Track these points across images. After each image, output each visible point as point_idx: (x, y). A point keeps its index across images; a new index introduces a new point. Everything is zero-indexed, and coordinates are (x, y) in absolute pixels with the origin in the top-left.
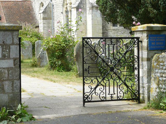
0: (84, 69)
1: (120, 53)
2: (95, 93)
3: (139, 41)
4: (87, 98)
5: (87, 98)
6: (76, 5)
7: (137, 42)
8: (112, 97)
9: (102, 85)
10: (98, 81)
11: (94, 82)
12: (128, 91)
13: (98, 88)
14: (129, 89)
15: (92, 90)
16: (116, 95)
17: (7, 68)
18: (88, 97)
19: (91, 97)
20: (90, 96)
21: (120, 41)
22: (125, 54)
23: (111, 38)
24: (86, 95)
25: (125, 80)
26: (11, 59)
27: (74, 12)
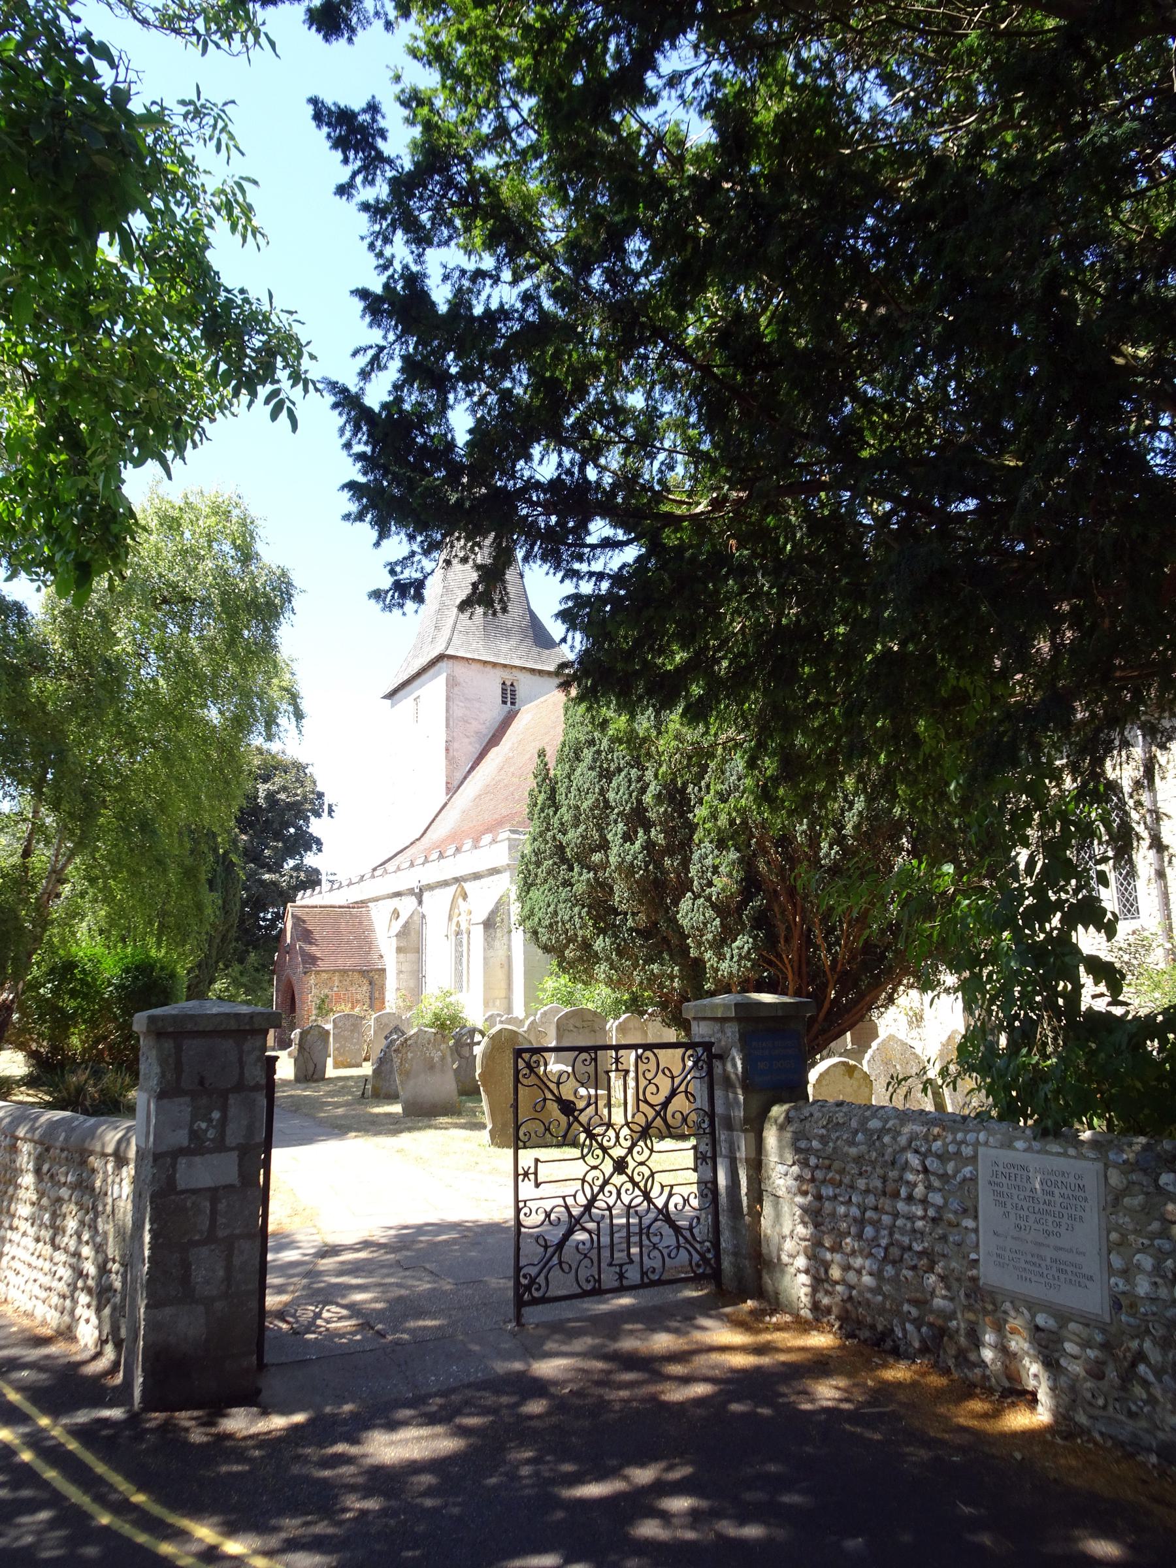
0: (521, 1171)
1: (646, 1101)
2: (673, 1078)
3: (711, 1057)
4: (528, 1288)
5: (528, 1288)
6: (484, 916)
7: (704, 1057)
8: (621, 1276)
9: (652, 1106)
10: (665, 1120)
11: (678, 1115)
12: (678, 1247)
13: (665, 1091)
14: (681, 1240)
15: (550, 1250)
16: (636, 1266)
17: (209, 1189)
18: (533, 1281)
19: (543, 1284)
20: (541, 1280)
21: (588, 1281)
22: (666, 1104)
23: (617, 1048)
24: (525, 1276)
25: (570, 1125)
26: (232, 1149)
27: (478, 932)
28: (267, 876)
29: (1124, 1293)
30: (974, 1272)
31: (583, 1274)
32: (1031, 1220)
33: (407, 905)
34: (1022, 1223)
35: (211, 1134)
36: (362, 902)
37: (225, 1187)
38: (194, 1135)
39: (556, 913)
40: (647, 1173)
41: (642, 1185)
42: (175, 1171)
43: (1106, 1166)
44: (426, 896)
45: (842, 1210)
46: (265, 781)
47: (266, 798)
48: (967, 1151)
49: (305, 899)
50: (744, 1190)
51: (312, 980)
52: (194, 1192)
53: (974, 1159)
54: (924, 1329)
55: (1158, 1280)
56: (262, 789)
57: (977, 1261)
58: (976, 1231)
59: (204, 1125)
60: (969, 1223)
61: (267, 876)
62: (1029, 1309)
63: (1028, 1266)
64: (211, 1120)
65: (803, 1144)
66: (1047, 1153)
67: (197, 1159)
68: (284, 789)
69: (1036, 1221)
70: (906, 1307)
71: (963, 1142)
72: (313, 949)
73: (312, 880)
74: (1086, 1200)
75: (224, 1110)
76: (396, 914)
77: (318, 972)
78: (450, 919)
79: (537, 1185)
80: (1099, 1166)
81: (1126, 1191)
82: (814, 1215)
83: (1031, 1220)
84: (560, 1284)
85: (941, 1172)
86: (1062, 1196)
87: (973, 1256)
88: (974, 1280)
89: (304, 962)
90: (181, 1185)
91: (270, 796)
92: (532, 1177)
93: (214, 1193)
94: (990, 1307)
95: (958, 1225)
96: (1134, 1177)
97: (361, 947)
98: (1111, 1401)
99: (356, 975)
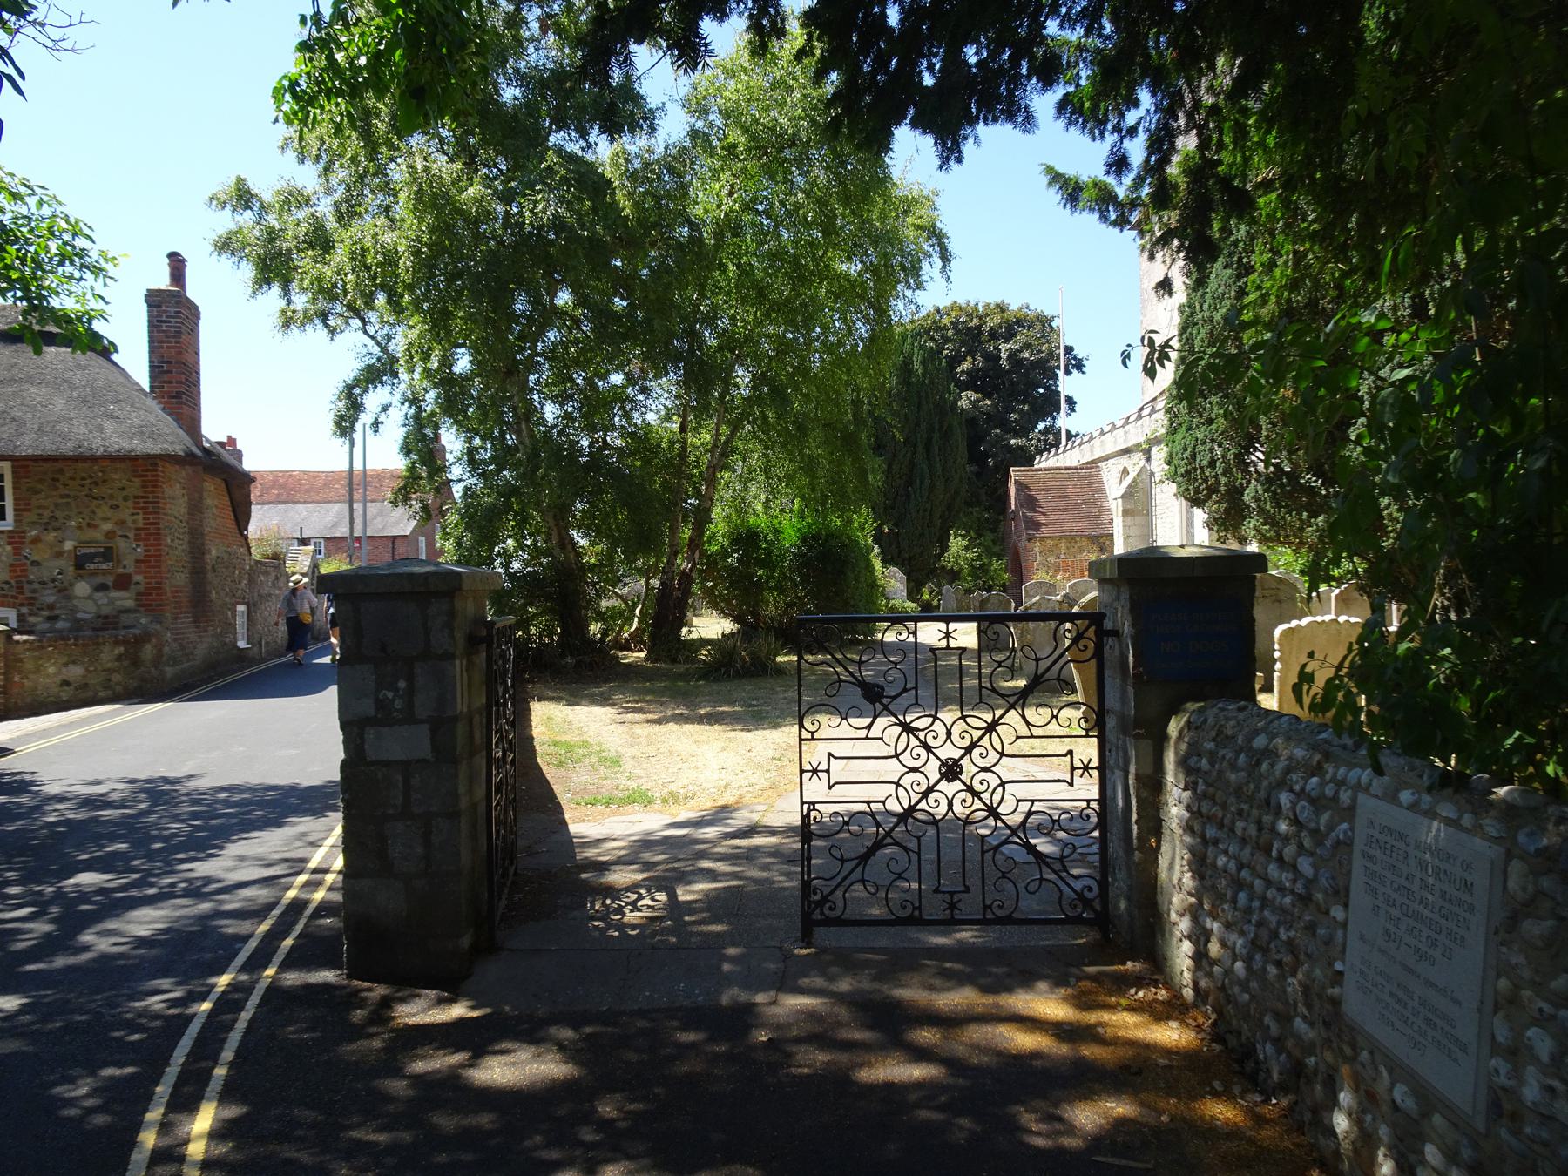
3: (1102, 634)
8: (952, 906)
19: (840, 904)
26: (422, 722)
28: (1013, 442)
29: (1504, 1089)
30: (1336, 991)
33: (1135, 463)
34: (1393, 929)
35: (398, 704)
36: (1093, 462)
37: (418, 761)
38: (381, 704)
39: (1193, 456)
40: (995, 781)
41: (985, 796)
42: (363, 741)
43: (1509, 856)
45: (1222, 860)
46: (1007, 341)
47: (1009, 357)
49: (1045, 462)
50: (1134, 817)
51: (1037, 547)
52: (387, 764)
53: (1350, 812)
55: (1556, 1084)
56: (1004, 348)
57: (1341, 973)
58: (1344, 925)
59: (390, 695)
60: (1338, 913)
61: (1013, 442)
62: (1390, 1072)
64: (397, 690)
65: (1192, 762)
67: (385, 730)
68: (1028, 346)
69: (1410, 931)
70: (1267, 1019)
72: (1037, 517)
73: (1052, 441)
74: (1472, 909)
75: (410, 679)
76: (1125, 472)
77: (1042, 539)
80: (1496, 851)
82: (1200, 865)
84: (861, 900)
85: (1312, 825)
87: (1338, 966)
89: (1027, 528)
90: (371, 755)
91: (1013, 355)
93: (406, 766)
94: (1348, 1051)
95: (1327, 913)
96: (1546, 883)
97: (1089, 511)
99: (1085, 541)
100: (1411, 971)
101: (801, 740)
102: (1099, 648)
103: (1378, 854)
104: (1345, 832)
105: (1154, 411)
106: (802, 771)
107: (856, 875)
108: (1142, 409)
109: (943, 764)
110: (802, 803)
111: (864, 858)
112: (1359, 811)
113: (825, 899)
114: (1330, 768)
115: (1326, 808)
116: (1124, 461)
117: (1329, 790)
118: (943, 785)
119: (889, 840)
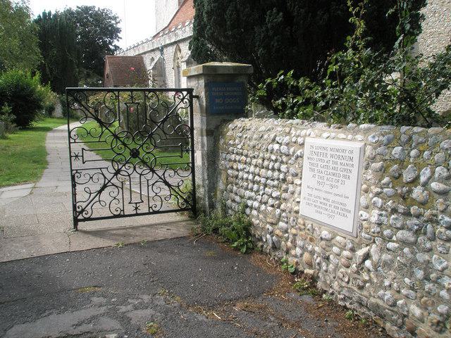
3: (192, 97)
15: (93, 196)
31: (114, 206)
32: (325, 179)
33: (157, 56)
44: (165, 50)
48: (300, 140)
53: (303, 145)
54: (274, 238)
58: (300, 185)
63: (321, 205)
66: (338, 139)
71: (299, 136)
78: (174, 60)
79: (84, 163)
81: (373, 159)
83: (325, 179)
86: (341, 164)
88: (297, 212)
92: (81, 158)
98: (351, 279)
100: (329, 193)
101: (70, 143)
102: (191, 102)
103: (315, 157)
104: (301, 153)
105: (184, 26)
106: (71, 157)
107: (97, 199)
108: (159, 33)
109: (132, 151)
110: (72, 170)
111: (105, 186)
112: (305, 144)
113: (83, 210)
114: (293, 132)
115: (292, 146)
116: (152, 55)
117: (294, 140)
118: (141, 156)
119: (110, 184)
